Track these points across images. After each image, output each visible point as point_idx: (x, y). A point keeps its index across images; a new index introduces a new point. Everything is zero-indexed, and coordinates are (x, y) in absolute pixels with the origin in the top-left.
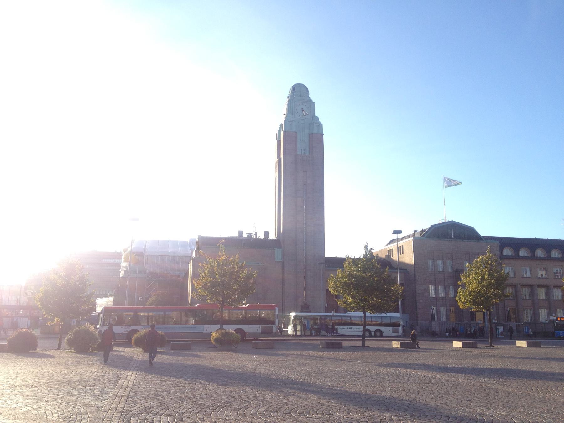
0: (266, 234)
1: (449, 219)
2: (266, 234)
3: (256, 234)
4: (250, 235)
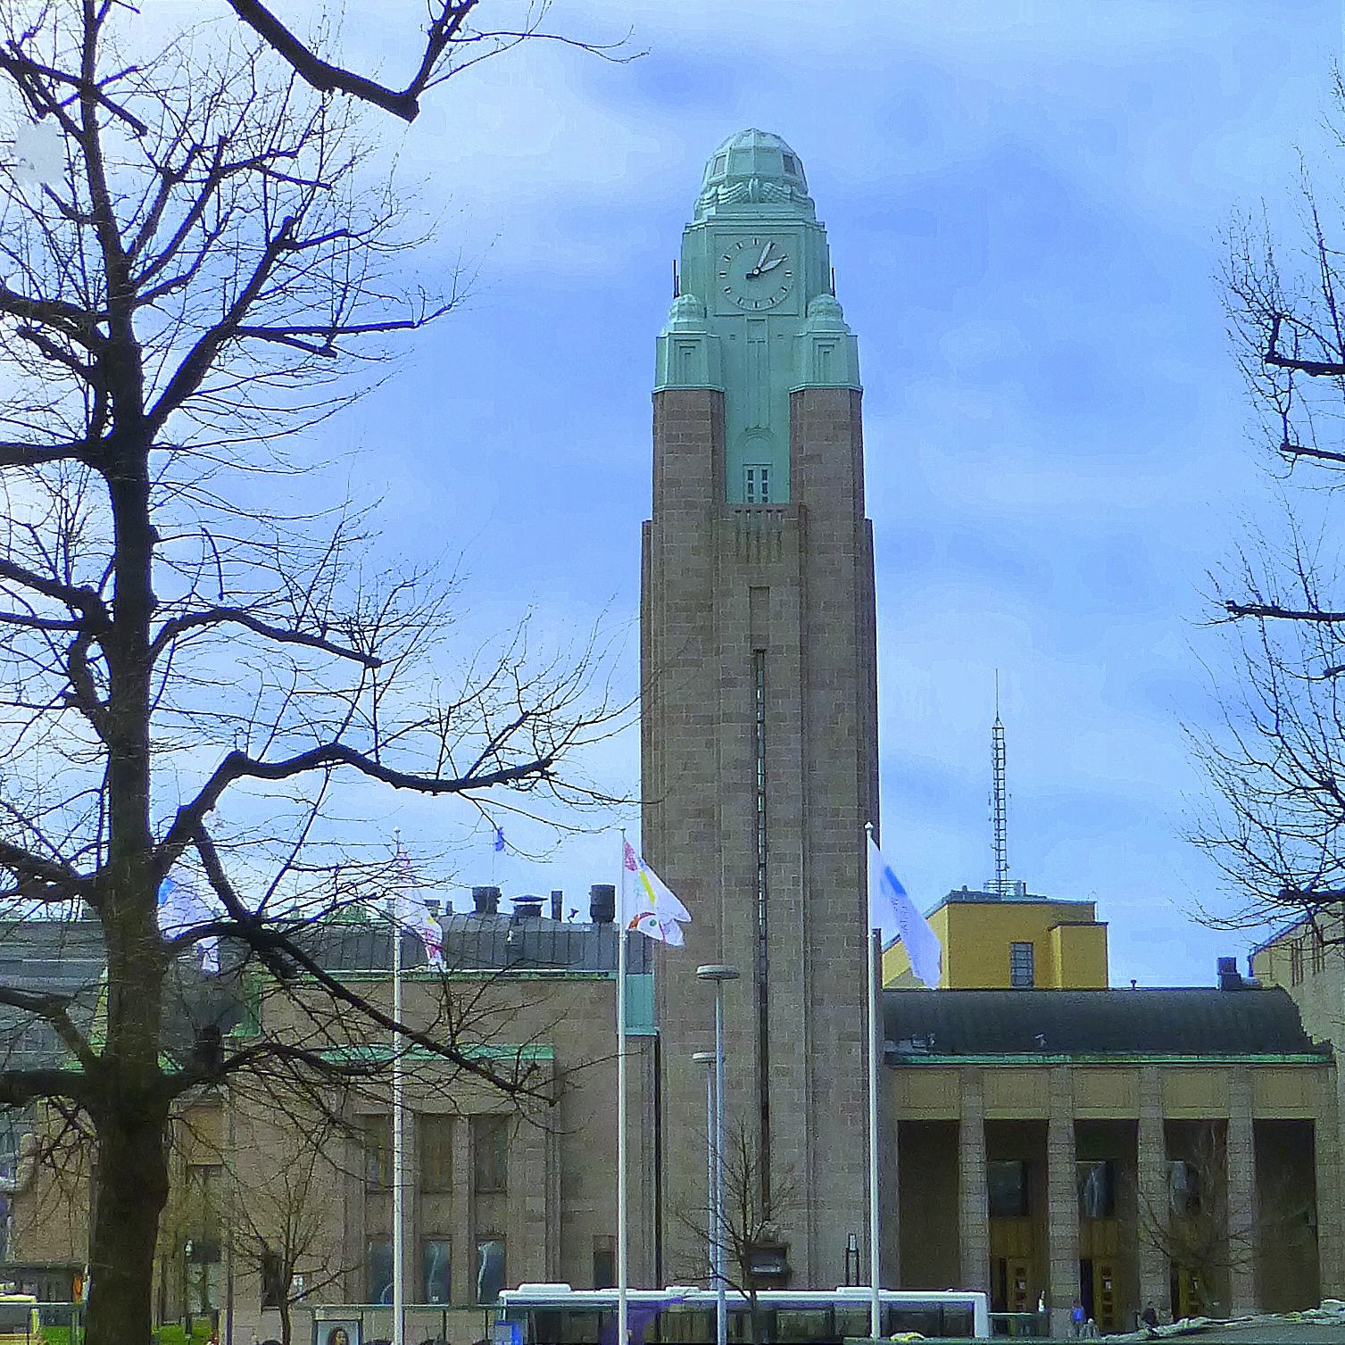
3: (557, 898)
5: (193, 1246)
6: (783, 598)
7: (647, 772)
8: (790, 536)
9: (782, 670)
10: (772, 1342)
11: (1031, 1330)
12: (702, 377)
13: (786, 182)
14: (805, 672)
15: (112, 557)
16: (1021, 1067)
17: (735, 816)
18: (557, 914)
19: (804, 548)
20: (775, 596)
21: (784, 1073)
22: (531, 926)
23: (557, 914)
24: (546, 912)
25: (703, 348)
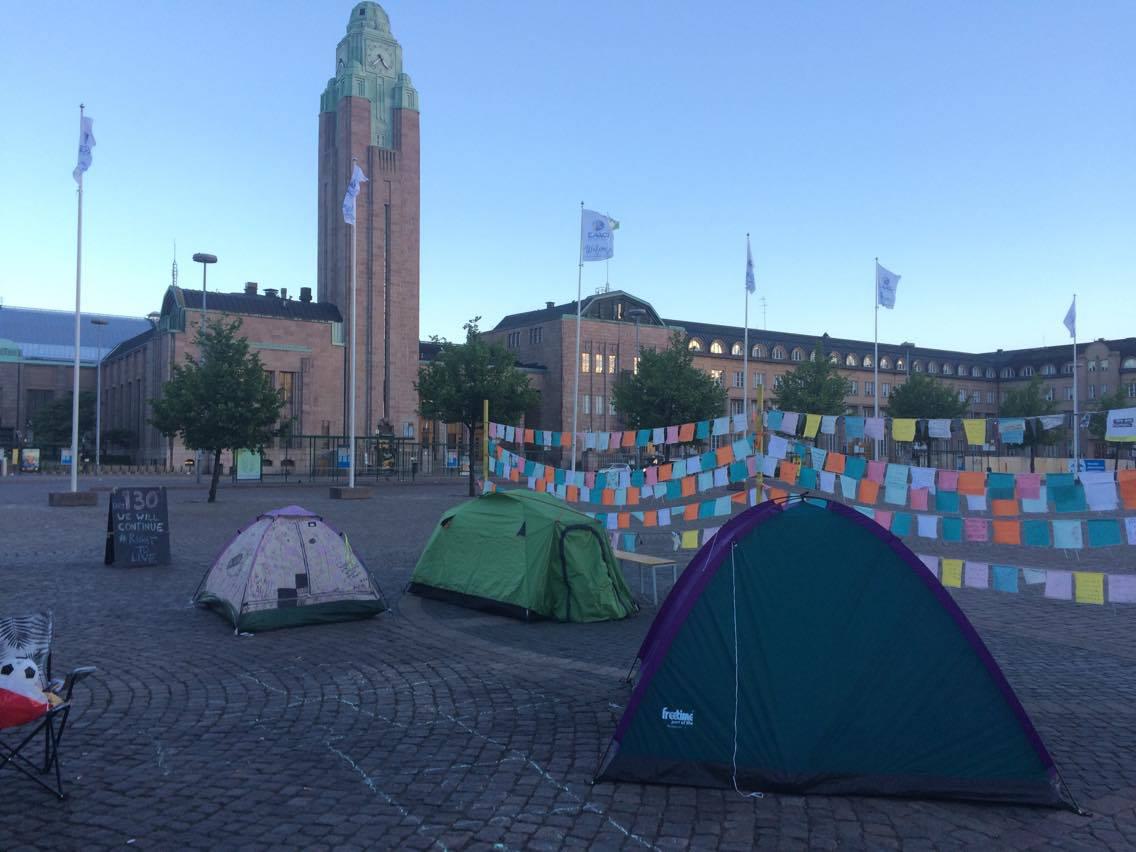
0: (306, 292)
1: (614, 288)
3: (284, 291)
4: (271, 293)
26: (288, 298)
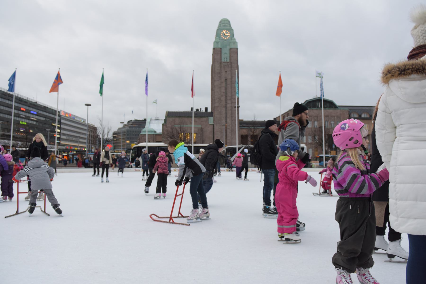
0: (206, 109)
2: (206, 109)
3: (201, 109)
5: (342, 255)
6: (229, 73)
7: (216, 83)
8: (230, 66)
9: (229, 81)
10: (143, 154)
11: (129, 153)
12: (220, 46)
13: (229, 24)
14: (231, 82)
15: (185, 165)
16: (315, 109)
17: (223, 99)
18: (201, 111)
19: (231, 67)
20: (228, 73)
21: (229, 129)
22: (198, 112)
23: (201, 111)
24: (199, 110)
25: (220, 43)
26: (202, 111)
